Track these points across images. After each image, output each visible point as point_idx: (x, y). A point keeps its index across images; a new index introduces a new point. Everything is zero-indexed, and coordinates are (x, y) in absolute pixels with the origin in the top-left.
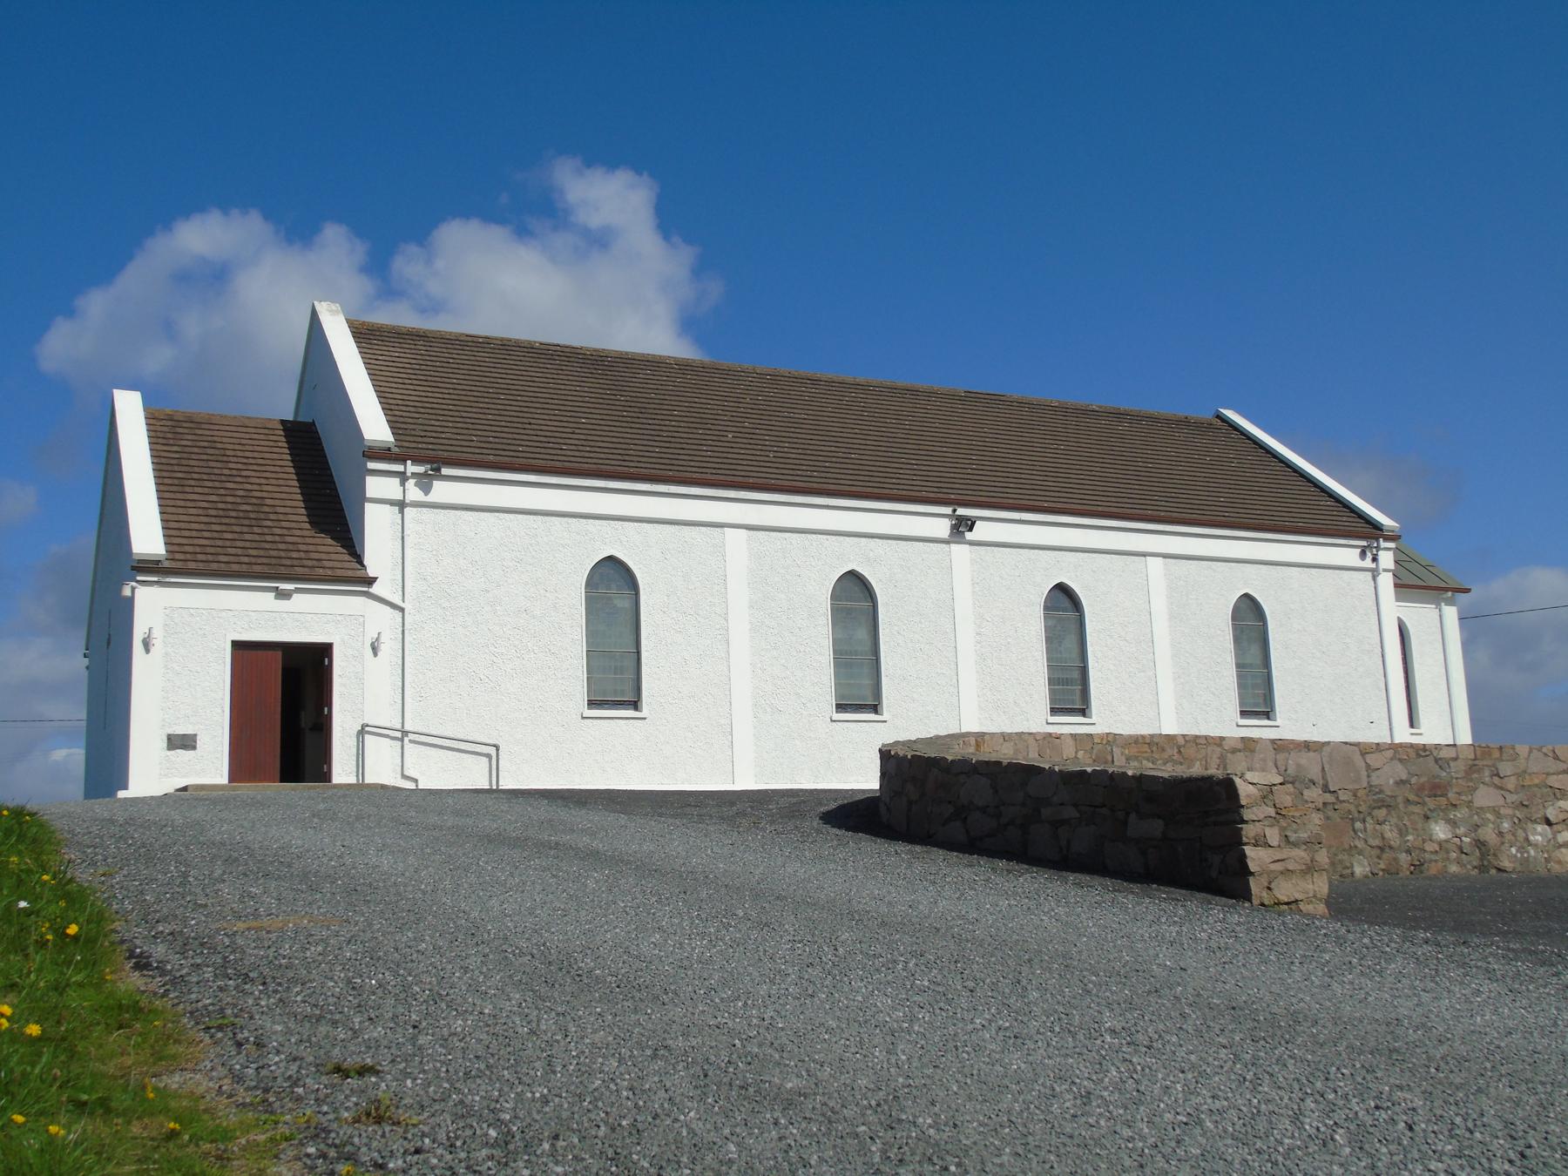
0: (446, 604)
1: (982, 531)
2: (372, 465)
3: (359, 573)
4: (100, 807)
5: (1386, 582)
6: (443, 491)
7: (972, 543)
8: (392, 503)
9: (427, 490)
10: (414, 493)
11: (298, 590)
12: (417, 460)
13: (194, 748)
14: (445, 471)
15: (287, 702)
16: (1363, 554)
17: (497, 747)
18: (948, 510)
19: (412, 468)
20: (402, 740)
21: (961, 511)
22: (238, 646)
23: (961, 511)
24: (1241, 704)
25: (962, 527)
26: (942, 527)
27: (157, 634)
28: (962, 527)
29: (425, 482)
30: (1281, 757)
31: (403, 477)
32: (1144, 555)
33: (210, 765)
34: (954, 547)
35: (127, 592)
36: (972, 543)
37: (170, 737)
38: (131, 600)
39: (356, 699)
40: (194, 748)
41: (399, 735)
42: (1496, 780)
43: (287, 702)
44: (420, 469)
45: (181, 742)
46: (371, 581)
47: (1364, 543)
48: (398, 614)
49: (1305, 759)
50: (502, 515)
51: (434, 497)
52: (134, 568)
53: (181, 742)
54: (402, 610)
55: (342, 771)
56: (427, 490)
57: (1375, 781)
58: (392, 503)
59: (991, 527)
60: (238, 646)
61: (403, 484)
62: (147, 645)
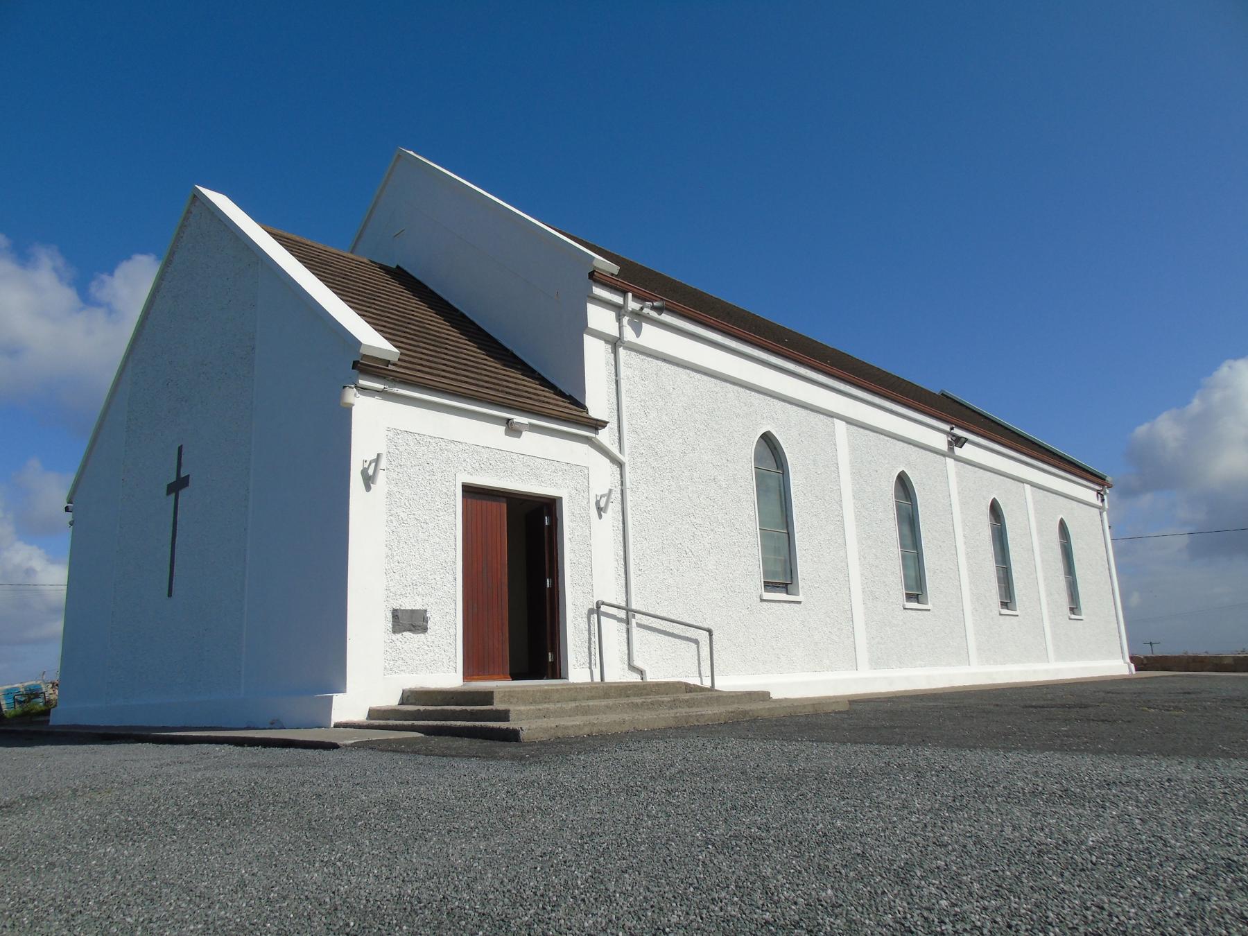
0: (654, 464)
1: (966, 451)
2: (598, 291)
6: (652, 337)
7: (958, 459)
11: (533, 428)
13: (425, 630)
14: (362, 382)
17: (710, 632)
18: (947, 427)
20: (628, 622)
21: (957, 432)
23: (957, 432)
24: (907, 587)
25: (958, 442)
29: (638, 319)
31: (619, 310)
33: (440, 664)
37: (396, 614)
39: (589, 569)
40: (425, 630)
41: (603, 608)
45: (409, 621)
48: (616, 469)
50: (693, 374)
52: (356, 365)
53: (409, 621)
54: (620, 465)
55: (578, 672)
61: (619, 320)
62: (368, 480)
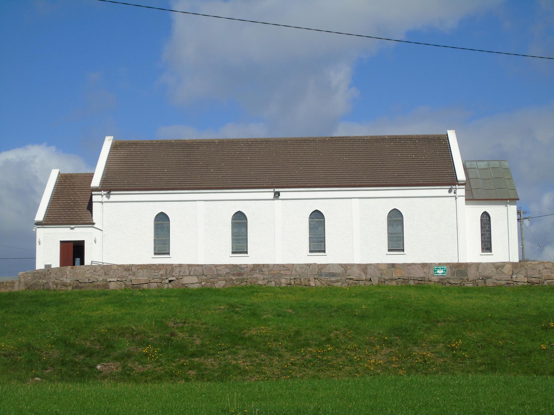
1: (282, 196)
2: (93, 193)
3: (91, 222)
4: (71, 274)
5: (462, 200)
6: (113, 198)
7: (282, 199)
8: (100, 202)
9: (109, 198)
10: (105, 199)
12: (104, 190)
14: (112, 192)
15: (74, 252)
16: (450, 191)
18: (272, 190)
19: (103, 192)
21: (276, 190)
22: (61, 242)
25: (277, 195)
26: (271, 195)
27: (42, 240)
28: (277, 195)
30: (190, 268)
32: (351, 198)
34: (275, 201)
35: (34, 230)
36: (282, 199)
38: (35, 232)
42: (261, 272)
43: (74, 252)
44: (105, 193)
46: (94, 224)
47: (450, 187)
49: (197, 268)
51: (110, 200)
56: (109, 198)
57: (219, 272)
58: (100, 202)
59: (285, 194)
60: (61, 242)
